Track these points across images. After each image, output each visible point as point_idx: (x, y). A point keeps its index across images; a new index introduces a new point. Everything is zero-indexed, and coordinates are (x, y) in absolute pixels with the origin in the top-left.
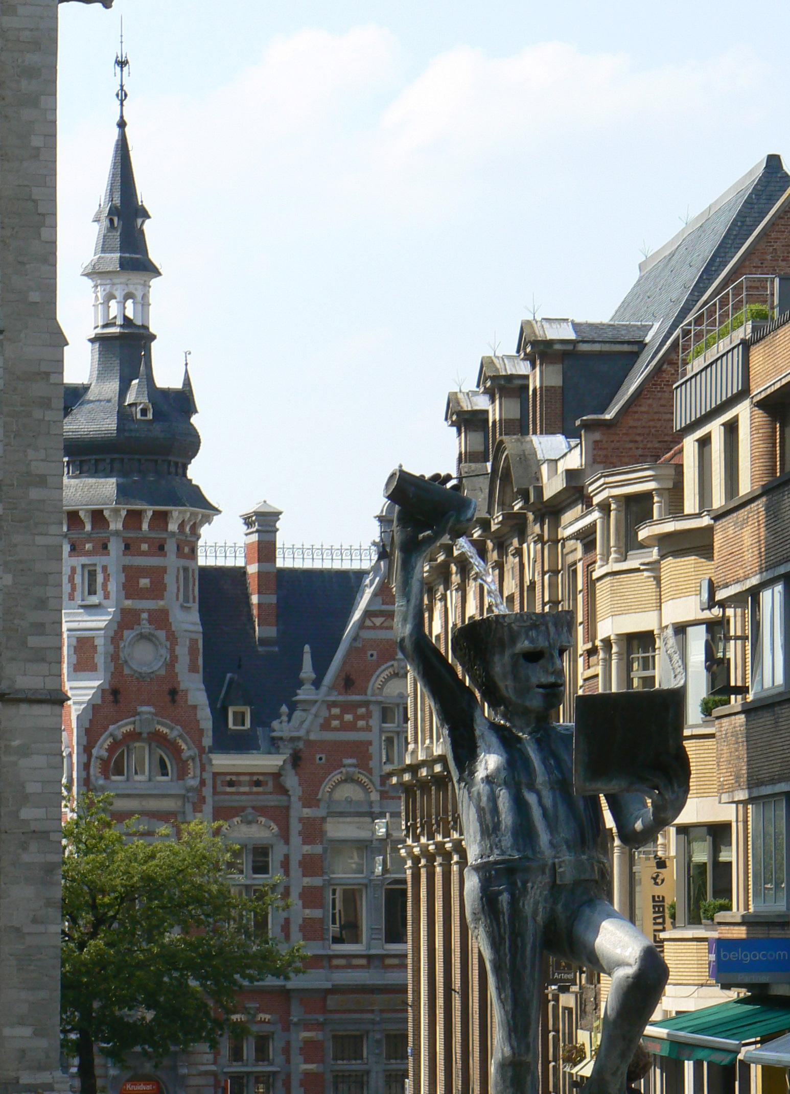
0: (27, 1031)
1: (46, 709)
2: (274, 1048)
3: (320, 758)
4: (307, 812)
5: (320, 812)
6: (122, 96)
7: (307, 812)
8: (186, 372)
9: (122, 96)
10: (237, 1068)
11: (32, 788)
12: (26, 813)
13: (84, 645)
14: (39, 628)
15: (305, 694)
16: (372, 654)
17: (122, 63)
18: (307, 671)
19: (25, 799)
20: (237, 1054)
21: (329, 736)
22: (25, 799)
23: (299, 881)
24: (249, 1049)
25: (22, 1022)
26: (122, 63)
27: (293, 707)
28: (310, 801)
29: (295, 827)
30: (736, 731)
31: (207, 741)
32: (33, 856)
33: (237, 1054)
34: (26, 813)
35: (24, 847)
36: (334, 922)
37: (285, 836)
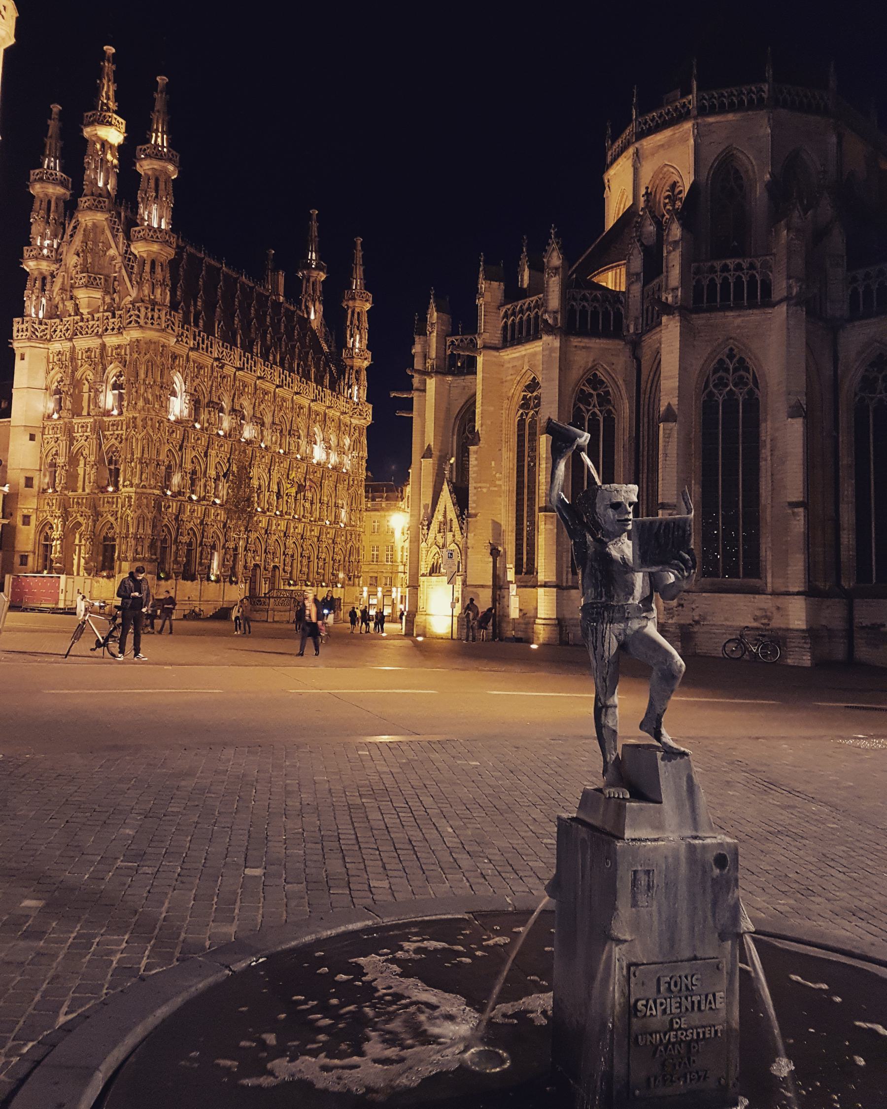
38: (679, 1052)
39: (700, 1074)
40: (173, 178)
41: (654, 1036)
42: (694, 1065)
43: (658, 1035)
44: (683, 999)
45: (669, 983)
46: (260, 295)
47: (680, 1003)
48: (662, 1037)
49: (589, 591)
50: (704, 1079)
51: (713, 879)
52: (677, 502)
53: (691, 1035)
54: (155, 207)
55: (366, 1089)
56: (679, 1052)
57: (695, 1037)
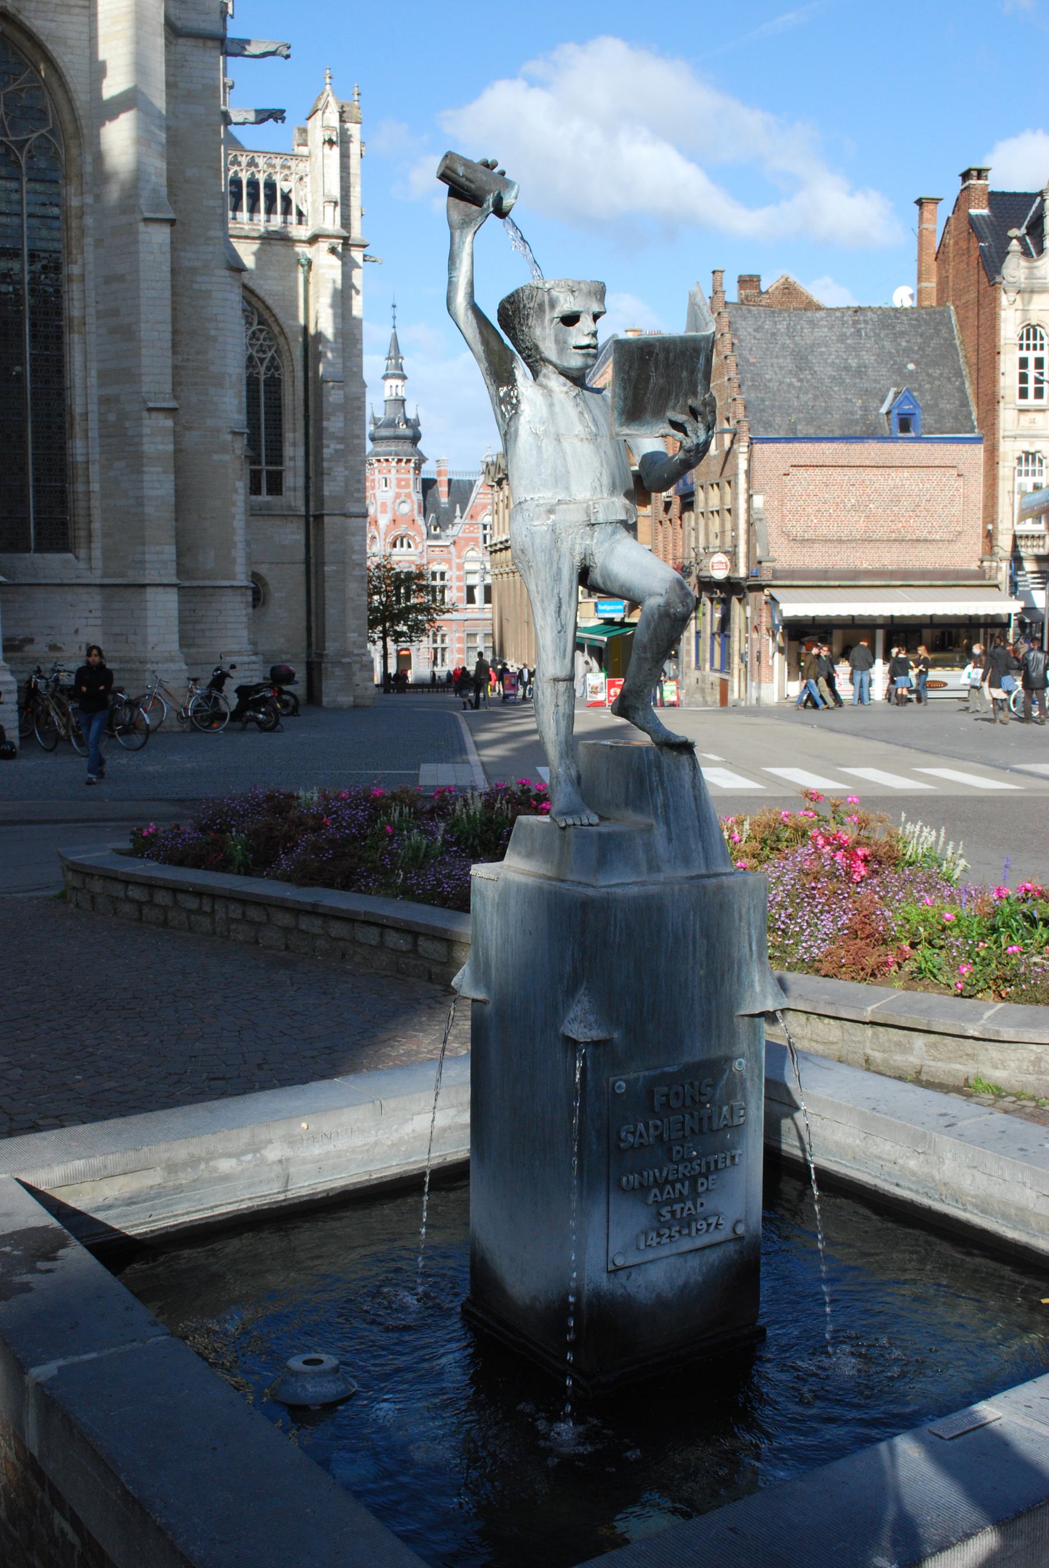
0: (356, 635)
1: (361, 519)
2: (447, 639)
3: (463, 542)
4: (458, 561)
5: (462, 561)
6: (394, 318)
7: (458, 561)
8: (395, 336)
9: (394, 318)
10: (435, 646)
11: (356, 548)
12: (355, 557)
13: (384, 505)
14: (358, 490)
15: (456, 521)
16: (479, 508)
17: (394, 306)
18: (458, 513)
19: (354, 552)
20: (435, 641)
21: (465, 535)
22: (354, 552)
23: (845, 917)
24: (439, 639)
25: (354, 632)
26: (394, 306)
27: (453, 525)
28: (459, 557)
29: (454, 566)
30: (1035, 339)
31: (425, 537)
32: (357, 572)
33: (435, 641)
34: (355, 557)
35: (354, 569)
36: (306, 1362)
37: (450, 568)
38: (681, 1193)
39: (710, 1221)
40: (973, 212)
41: (645, 1173)
42: (702, 1209)
43: (651, 1173)
44: (687, 1116)
45: (667, 1096)
46: (980, 239)
47: (683, 1123)
48: (657, 1174)
49: (411, 1300)
50: (716, 1227)
51: (72, 692)
52: (338, 709)
53: (697, 1167)
54: (268, 273)
55: (577, 1288)
56: (681, 1193)
57: (704, 1170)
